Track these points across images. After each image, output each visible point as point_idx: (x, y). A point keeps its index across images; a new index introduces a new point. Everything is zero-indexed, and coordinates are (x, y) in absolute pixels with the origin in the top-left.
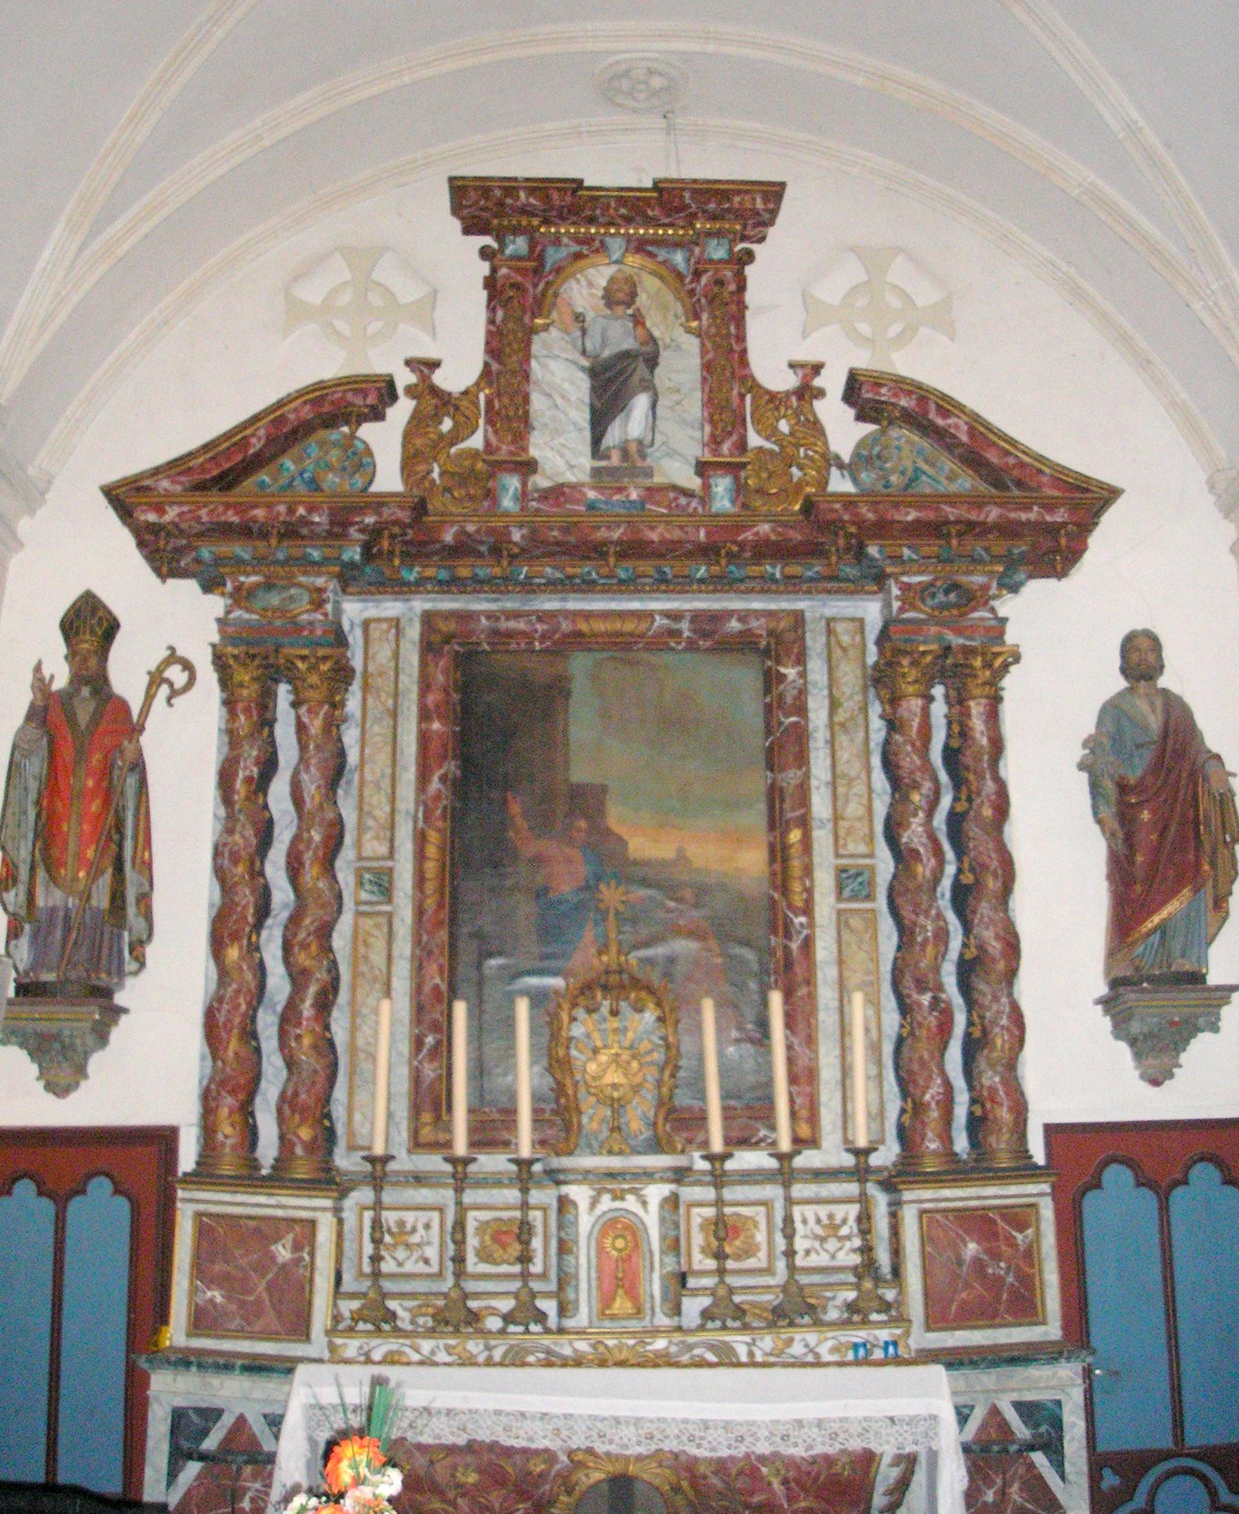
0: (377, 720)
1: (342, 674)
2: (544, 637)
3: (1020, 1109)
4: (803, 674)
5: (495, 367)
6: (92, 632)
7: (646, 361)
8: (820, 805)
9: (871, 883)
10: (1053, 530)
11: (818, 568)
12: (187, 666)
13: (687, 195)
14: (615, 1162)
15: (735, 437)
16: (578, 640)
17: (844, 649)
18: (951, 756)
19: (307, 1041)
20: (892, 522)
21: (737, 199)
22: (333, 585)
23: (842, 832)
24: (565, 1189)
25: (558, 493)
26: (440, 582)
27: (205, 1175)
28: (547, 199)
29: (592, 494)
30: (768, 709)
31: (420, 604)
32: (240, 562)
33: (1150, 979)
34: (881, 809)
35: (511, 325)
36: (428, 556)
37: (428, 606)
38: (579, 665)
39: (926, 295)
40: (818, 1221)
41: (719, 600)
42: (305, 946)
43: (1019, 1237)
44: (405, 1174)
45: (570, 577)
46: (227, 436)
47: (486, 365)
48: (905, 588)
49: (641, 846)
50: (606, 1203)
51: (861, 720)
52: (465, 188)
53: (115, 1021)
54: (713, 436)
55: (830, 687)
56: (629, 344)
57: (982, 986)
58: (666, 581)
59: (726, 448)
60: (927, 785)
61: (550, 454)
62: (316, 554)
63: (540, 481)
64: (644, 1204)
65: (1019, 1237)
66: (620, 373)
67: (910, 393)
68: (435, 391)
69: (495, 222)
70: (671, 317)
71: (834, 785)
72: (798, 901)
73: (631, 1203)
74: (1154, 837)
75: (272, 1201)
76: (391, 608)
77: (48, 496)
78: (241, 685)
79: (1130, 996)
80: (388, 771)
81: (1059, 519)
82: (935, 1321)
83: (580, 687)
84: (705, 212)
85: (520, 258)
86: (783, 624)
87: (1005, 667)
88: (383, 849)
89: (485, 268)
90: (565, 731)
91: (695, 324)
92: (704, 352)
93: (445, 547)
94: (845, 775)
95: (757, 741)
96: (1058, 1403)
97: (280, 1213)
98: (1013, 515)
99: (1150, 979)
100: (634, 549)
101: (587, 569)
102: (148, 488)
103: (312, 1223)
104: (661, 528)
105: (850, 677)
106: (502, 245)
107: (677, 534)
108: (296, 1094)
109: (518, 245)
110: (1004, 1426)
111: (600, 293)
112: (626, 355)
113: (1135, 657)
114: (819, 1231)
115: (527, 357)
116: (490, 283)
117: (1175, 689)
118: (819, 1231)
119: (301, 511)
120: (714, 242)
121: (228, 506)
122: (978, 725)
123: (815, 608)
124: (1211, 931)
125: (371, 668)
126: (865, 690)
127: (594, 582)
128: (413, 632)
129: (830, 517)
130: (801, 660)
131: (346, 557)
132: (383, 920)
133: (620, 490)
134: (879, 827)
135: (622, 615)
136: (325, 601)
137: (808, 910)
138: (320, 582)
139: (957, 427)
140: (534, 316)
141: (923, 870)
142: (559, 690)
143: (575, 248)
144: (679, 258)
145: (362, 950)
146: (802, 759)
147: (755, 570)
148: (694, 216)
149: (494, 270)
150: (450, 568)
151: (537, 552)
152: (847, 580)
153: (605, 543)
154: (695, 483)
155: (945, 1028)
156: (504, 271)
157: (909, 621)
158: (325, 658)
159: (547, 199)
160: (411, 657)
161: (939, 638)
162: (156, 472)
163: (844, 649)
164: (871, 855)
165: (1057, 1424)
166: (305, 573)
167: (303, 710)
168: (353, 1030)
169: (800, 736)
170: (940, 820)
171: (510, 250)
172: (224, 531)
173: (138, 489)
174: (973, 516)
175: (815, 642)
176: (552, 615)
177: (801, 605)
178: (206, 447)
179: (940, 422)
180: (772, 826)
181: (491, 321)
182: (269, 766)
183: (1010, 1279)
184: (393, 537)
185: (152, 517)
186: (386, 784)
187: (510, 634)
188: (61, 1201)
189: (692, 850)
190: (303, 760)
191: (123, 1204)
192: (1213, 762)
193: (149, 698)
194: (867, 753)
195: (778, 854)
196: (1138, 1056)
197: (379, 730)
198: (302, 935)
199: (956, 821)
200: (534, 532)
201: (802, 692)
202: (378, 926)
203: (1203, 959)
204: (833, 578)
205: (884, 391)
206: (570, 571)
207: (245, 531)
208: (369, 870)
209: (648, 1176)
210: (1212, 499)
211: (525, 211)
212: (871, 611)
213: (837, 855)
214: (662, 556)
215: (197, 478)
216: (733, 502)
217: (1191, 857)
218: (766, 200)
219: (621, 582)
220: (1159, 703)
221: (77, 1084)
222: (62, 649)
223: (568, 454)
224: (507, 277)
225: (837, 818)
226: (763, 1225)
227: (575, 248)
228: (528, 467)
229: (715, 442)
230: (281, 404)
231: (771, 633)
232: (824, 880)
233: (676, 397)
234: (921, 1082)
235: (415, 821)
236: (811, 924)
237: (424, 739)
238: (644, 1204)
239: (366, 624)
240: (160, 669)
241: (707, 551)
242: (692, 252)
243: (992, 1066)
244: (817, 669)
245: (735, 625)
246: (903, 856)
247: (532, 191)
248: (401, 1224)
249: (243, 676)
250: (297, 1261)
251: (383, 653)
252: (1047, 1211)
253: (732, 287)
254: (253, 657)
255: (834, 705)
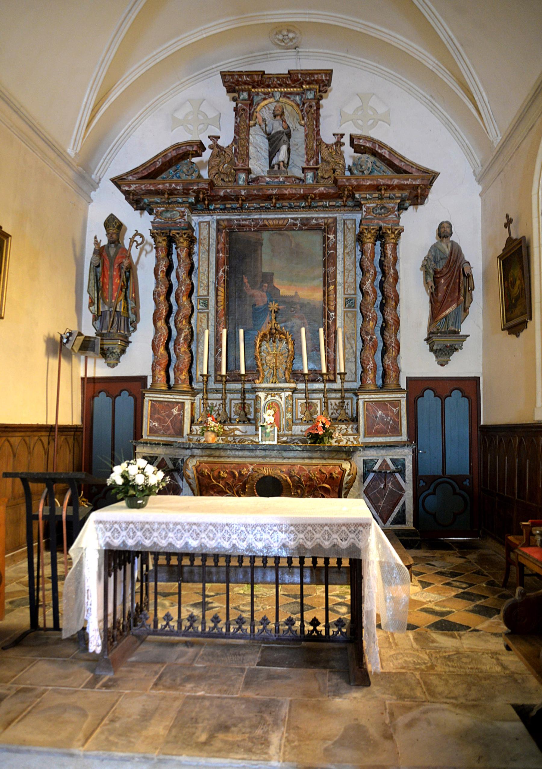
0: (203, 253)
1: (192, 241)
2: (254, 227)
3: (398, 371)
4: (335, 237)
5: (237, 137)
6: (114, 227)
7: (286, 134)
8: (340, 279)
9: (355, 303)
10: (415, 187)
11: (340, 203)
12: (142, 236)
13: (299, 75)
14: (272, 385)
15: (314, 159)
16: (265, 227)
17: (349, 229)
18: (381, 263)
19: (182, 350)
20: (362, 185)
21: (316, 76)
22: (187, 210)
23: (346, 287)
24: (257, 393)
25: (256, 180)
26: (221, 209)
27: (153, 390)
28: (252, 78)
29: (268, 179)
30: (324, 248)
31: (215, 217)
32: (157, 203)
33: (441, 333)
34: (359, 280)
35: (242, 123)
36: (217, 200)
37: (219, 217)
38: (265, 235)
39: (382, 109)
40: (336, 404)
41: (309, 214)
42: (181, 322)
43: (395, 410)
44: (213, 389)
45: (262, 207)
46: (149, 161)
47: (235, 137)
48: (368, 208)
49: (284, 292)
50: (269, 398)
51: (353, 252)
52: (225, 75)
53: (128, 345)
54: (307, 159)
55: (344, 241)
56: (281, 129)
57: (387, 334)
58: (292, 208)
59: (311, 163)
60: (372, 271)
61: (256, 167)
62: (180, 200)
63: (252, 176)
64: (281, 398)
65: (395, 410)
66: (277, 138)
67: (370, 141)
68: (218, 146)
69: (237, 87)
70: (295, 119)
71: (344, 272)
72: (332, 308)
73: (277, 398)
74: (445, 288)
75: (172, 397)
76: (207, 218)
77: (100, 185)
78: (159, 242)
79: (434, 338)
80: (207, 269)
81: (417, 183)
82: (369, 433)
83: (265, 242)
84: (306, 81)
85: (245, 100)
86: (329, 221)
87: (399, 234)
88: (206, 293)
89: (234, 104)
90: (261, 257)
91: (302, 122)
92: (305, 131)
93: (221, 197)
94: (348, 269)
95: (321, 259)
96: (404, 459)
97: (174, 400)
98: (402, 182)
99: (441, 333)
100: (281, 197)
101: (267, 204)
102: (125, 179)
103: (183, 403)
104: (288, 190)
105: (351, 238)
106: (239, 96)
107: (294, 191)
108: (178, 366)
109: (245, 95)
110: (387, 465)
111: (272, 112)
112: (279, 132)
113: (442, 230)
114: (336, 407)
115: (248, 134)
116: (235, 110)
117: (456, 241)
118: (336, 407)
119: (174, 185)
120: (309, 92)
121: (150, 184)
122: (389, 252)
123: (340, 216)
124: (463, 318)
125: (201, 237)
126: (355, 242)
127: (269, 208)
128: (214, 226)
129: (342, 184)
130: (335, 233)
131: (190, 201)
132: (206, 314)
133: (277, 177)
134: (358, 286)
135: (279, 219)
136: (184, 215)
137: (335, 311)
138: (183, 209)
139: (385, 153)
140: (250, 120)
141: (370, 298)
142: (259, 243)
143: (263, 96)
144: (298, 98)
145: (199, 323)
146: (335, 264)
147: (320, 204)
148: (302, 83)
149: (237, 105)
150: (223, 204)
151: (251, 198)
152: (350, 206)
153: (271, 195)
154: (302, 176)
155: (375, 347)
156: (240, 105)
157: (369, 219)
158: (185, 234)
159: (252, 78)
160: (213, 233)
161: (378, 223)
162: (128, 174)
163: (349, 229)
164: (355, 294)
165: (404, 465)
166: (178, 207)
167: (179, 250)
168: (197, 347)
169: (334, 257)
170: (377, 283)
171: (242, 97)
172: (150, 193)
173: (122, 179)
174: (389, 183)
175: (340, 227)
176: (256, 219)
177: (335, 215)
178: (142, 165)
179: (379, 151)
180: (324, 285)
181: (236, 122)
182: (170, 268)
183: (391, 422)
184: (204, 194)
185: (127, 188)
186: (206, 273)
187: (244, 226)
188: (114, 397)
189: (300, 293)
190: (179, 265)
191: (131, 398)
192: (466, 265)
193: (131, 246)
194: (355, 263)
195: (326, 294)
196: (437, 357)
197: (204, 256)
198: (179, 319)
199: (382, 283)
200: (248, 191)
201: (335, 243)
202: (204, 316)
203: (459, 327)
204: (345, 206)
205: (361, 141)
206: (262, 205)
207: (158, 193)
208: (201, 299)
209: (282, 389)
210: (474, 178)
211: (246, 83)
212: (358, 217)
213: (345, 294)
214: (291, 199)
215: (140, 175)
216: (313, 181)
217: (457, 294)
218: (326, 76)
219: (278, 208)
220: (450, 245)
221: (117, 364)
222: (105, 232)
223: (262, 167)
224: (241, 107)
225: (345, 283)
226: (319, 405)
227: (263, 96)
228: (248, 171)
229: (308, 161)
230: (166, 151)
231: (325, 224)
232: (340, 302)
233: (297, 147)
234: (366, 362)
235: (215, 284)
236: (335, 315)
237: (217, 259)
238: (281, 398)
239: (199, 223)
240: (133, 238)
241: (304, 197)
242: (302, 97)
243: (389, 358)
244: (340, 236)
245: (314, 221)
246: (364, 293)
247: (247, 76)
248: (212, 404)
249: (160, 239)
250: (179, 414)
251: (205, 233)
252: (404, 403)
253: (315, 108)
254: (163, 233)
255: (345, 247)
